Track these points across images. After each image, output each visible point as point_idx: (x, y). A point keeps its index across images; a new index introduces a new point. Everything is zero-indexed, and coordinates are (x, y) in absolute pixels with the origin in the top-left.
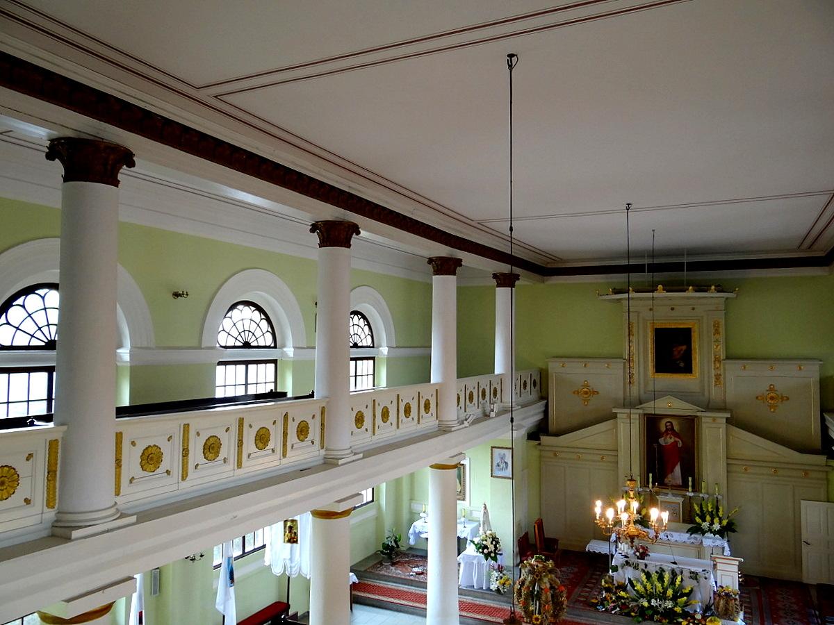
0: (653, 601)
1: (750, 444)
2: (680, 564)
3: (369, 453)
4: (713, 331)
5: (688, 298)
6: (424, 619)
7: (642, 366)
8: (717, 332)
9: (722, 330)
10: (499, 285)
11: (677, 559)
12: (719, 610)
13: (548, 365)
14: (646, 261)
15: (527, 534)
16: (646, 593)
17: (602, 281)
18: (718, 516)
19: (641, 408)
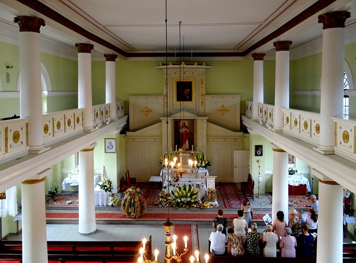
0: (182, 199)
1: (216, 130)
2: (192, 182)
3: (54, 146)
4: (200, 83)
5: (194, 68)
6: (77, 225)
7: (171, 98)
8: (202, 83)
9: (204, 82)
10: (107, 60)
11: (191, 180)
12: (209, 198)
13: (129, 99)
14: (175, 52)
15: (123, 177)
16: (179, 196)
17: (153, 60)
18: (204, 160)
19: (172, 117)
